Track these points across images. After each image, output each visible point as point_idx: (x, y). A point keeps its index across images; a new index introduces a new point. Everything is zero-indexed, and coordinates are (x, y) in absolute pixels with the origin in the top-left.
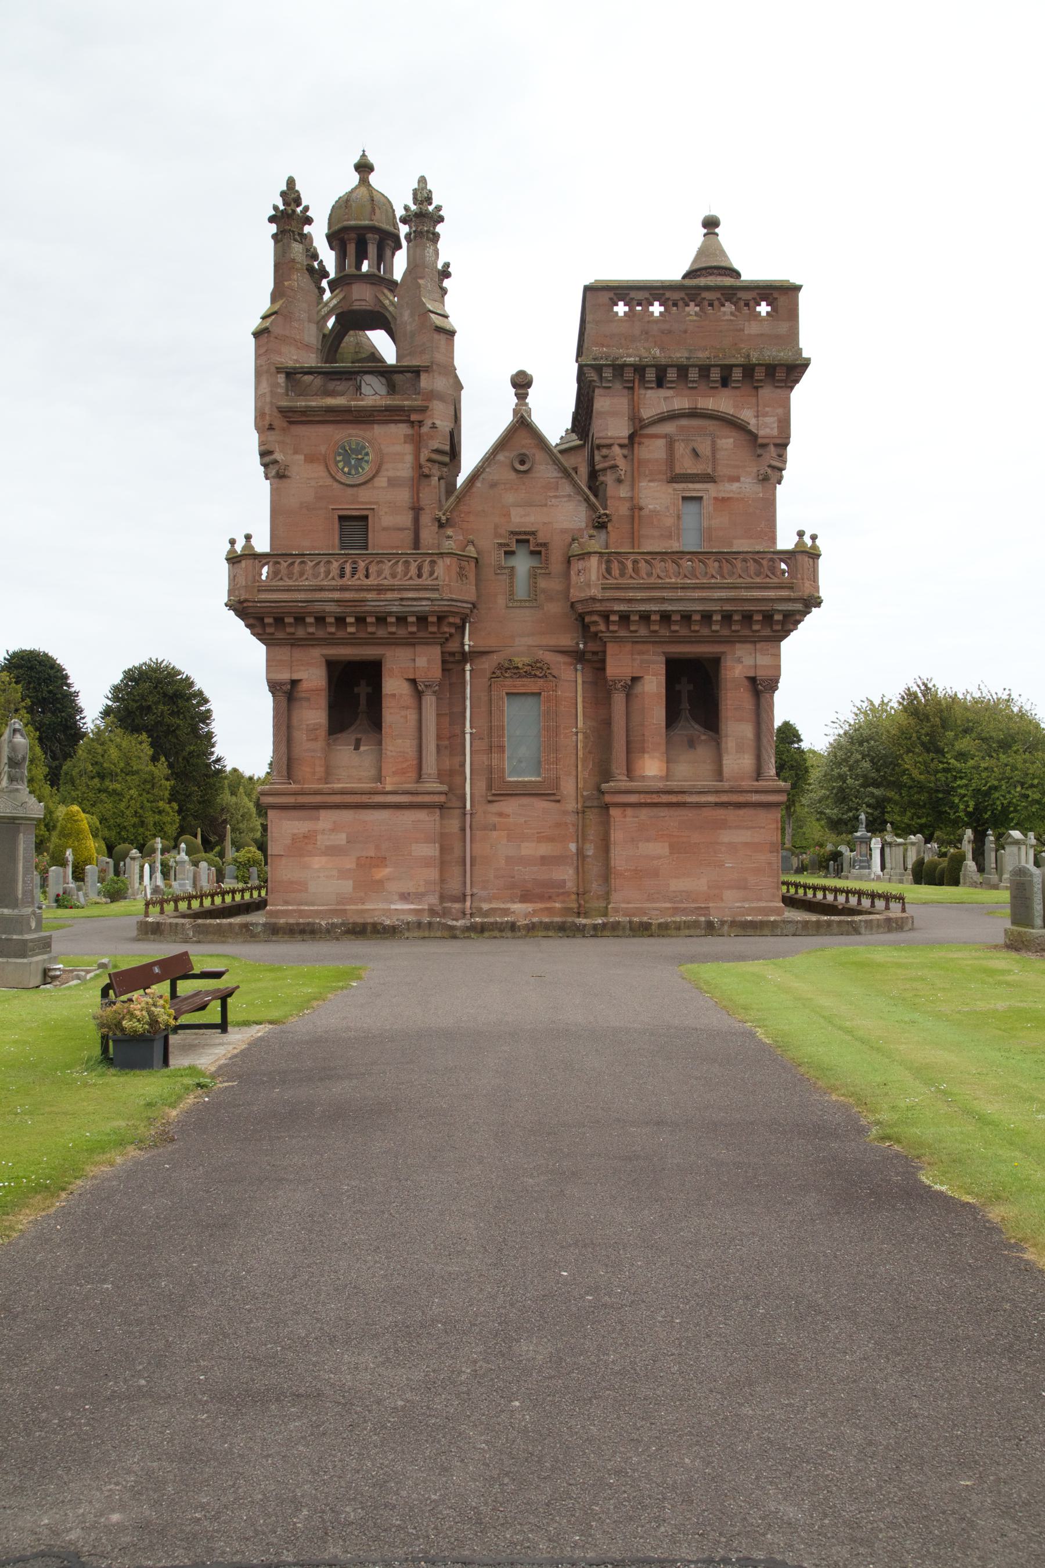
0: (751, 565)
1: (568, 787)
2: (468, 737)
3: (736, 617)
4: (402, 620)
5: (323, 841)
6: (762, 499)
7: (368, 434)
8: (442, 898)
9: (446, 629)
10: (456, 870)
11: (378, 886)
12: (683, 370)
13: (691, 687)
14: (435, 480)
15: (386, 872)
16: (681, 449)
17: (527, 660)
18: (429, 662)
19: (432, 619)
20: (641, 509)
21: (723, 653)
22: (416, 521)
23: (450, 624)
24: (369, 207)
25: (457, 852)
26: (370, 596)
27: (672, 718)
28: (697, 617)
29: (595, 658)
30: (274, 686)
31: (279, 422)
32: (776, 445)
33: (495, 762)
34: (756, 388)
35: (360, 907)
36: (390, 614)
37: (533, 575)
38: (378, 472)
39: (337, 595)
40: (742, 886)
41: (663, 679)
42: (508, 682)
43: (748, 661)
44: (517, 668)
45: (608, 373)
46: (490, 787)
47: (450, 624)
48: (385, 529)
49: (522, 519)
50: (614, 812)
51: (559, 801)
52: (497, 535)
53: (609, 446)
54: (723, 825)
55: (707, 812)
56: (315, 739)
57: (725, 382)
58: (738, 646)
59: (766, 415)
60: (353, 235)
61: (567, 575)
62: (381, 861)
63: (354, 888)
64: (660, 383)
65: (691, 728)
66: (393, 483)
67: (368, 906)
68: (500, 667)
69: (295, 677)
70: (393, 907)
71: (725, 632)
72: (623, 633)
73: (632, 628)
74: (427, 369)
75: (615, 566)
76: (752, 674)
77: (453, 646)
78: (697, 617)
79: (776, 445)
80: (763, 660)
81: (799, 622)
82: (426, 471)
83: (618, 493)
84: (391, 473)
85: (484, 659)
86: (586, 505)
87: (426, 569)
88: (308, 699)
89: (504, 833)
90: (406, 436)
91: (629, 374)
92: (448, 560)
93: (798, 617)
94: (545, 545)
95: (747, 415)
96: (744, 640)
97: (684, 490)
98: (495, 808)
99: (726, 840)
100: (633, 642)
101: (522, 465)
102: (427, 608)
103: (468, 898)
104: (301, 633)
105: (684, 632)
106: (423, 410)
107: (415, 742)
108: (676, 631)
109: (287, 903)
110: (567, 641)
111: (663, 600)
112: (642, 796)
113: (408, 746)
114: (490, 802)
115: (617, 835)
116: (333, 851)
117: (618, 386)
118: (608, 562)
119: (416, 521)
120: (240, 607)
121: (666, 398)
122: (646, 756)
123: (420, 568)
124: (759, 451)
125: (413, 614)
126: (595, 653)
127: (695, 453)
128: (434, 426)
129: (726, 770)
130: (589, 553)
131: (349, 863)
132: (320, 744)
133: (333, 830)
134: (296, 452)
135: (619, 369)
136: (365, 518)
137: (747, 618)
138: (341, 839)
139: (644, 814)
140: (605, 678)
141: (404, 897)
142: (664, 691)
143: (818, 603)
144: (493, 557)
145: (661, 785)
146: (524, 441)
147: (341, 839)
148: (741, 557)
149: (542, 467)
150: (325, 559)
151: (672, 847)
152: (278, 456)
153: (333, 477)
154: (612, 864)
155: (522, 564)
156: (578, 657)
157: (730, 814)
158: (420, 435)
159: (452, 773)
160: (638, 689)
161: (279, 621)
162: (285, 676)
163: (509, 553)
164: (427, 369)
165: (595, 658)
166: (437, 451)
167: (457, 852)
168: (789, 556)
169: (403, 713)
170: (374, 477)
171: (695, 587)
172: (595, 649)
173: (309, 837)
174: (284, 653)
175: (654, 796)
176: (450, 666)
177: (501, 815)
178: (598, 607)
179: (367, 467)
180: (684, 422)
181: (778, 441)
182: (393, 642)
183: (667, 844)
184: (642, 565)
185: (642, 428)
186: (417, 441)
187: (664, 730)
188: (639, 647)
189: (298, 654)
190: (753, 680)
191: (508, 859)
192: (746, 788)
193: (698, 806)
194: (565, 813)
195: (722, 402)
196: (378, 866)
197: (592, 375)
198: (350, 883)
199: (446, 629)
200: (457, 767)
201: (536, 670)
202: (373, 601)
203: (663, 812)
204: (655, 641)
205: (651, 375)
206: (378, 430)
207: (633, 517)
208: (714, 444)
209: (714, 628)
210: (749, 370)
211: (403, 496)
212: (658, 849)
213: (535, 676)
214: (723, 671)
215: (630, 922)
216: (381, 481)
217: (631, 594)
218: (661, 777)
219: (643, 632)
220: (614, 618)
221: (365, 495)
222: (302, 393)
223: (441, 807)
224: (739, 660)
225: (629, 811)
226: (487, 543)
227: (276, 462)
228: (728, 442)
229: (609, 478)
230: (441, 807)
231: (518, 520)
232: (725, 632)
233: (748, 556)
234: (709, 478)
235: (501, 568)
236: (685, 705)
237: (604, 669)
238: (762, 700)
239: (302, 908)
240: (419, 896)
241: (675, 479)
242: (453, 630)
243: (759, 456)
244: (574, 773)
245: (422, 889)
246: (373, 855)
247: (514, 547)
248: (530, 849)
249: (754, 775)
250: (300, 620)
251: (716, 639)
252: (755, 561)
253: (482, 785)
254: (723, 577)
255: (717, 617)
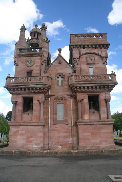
0: (104, 77)
1: (69, 121)
2: (49, 112)
3: (102, 87)
4: (36, 89)
5: (20, 132)
6: (104, 67)
7: (33, 58)
8: (44, 144)
9: (45, 91)
10: (47, 139)
11: (31, 142)
12: (88, 46)
13: (92, 103)
14: (44, 65)
15: (32, 139)
16: (88, 59)
17: (61, 97)
18: (42, 97)
19: (42, 89)
20: (82, 69)
21: (99, 94)
22: (40, 72)
23: (46, 90)
24: (36, 29)
25: (47, 135)
26: (30, 84)
27: (90, 108)
28: (94, 87)
29: (74, 96)
30: (13, 102)
31: (17, 57)
32: (106, 58)
33: (55, 117)
34: (101, 49)
35: (27, 146)
36: (34, 88)
37: (62, 81)
38: (34, 64)
39: (24, 84)
40: (106, 141)
41: (88, 100)
42: (57, 101)
43: (104, 96)
44: (59, 98)
45: (75, 46)
46: (54, 122)
47: (46, 90)
48: (35, 74)
49: (60, 71)
50: (79, 126)
51: (68, 124)
52: (55, 74)
53: (75, 58)
54: (101, 128)
55: (98, 126)
56: (20, 112)
57: (95, 48)
58: (102, 93)
59: (103, 53)
60: (33, 33)
61: (68, 81)
62: (31, 137)
63: (26, 142)
64: (84, 48)
65: (92, 110)
66: (36, 66)
67: (29, 146)
68: (56, 98)
69: (17, 100)
70: (34, 146)
71: (99, 90)
72: (79, 91)
73: (82, 90)
74: (43, 47)
75: (78, 78)
76: (105, 98)
77: (47, 94)
78: (94, 87)
79: (106, 58)
80: (107, 95)
81: (113, 88)
82: (42, 64)
83: (77, 67)
84: (36, 64)
85: (53, 97)
86: (71, 69)
87: (41, 79)
88: (19, 104)
89: (56, 131)
90: (39, 58)
91: (78, 46)
92: (45, 77)
93: (113, 87)
94: (64, 76)
95: (100, 53)
96: (103, 92)
97: (89, 66)
98: (54, 126)
99: (102, 131)
100: (82, 93)
101: (60, 62)
102: (41, 86)
103: (49, 145)
104: (18, 92)
105: (91, 90)
106: (42, 54)
107: (39, 113)
108: (90, 90)
109: (12, 145)
110: (69, 93)
111: (87, 84)
112: (85, 123)
113: (38, 114)
114: (54, 125)
115: (80, 131)
116: (22, 135)
117: (76, 49)
118: (76, 77)
119: (40, 72)
120: (8, 87)
121: (85, 51)
122: (85, 115)
123: (40, 79)
124: (103, 59)
125: (39, 87)
126: (74, 95)
127: (91, 59)
128: (44, 56)
129: (101, 117)
130: (72, 75)
131: (25, 137)
132: (20, 113)
133: (22, 130)
134: (20, 62)
135: (76, 46)
136: (31, 72)
137: (104, 87)
138: (23, 132)
139: (85, 126)
140: (77, 100)
141: (36, 144)
142: (88, 102)
143: (117, 84)
144: (54, 78)
145: (88, 121)
146: (60, 59)
147: (23, 132)
148: (102, 75)
149: (64, 63)
150: (22, 78)
151: (91, 133)
152: (16, 62)
153: (26, 65)
154: (79, 137)
155: (60, 79)
156: (71, 96)
157: (103, 126)
158: (42, 58)
159: (46, 119)
160: (83, 102)
161: (14, 89)
162: (15, 100)
163: (58, 78)
164: (43, 47)
165: (74, 96)
166: (44, 60)
167: (47, 135)
168: (110, 75)
169: (37, 107)
170: (33, 65)
171: (93, 81)
172: (74, 94)
173: (17, 132)
174: (15, 96)
175: (87, 123)
176: (46, 99)
177: (56, 127)
178: (74, 85)
179: (32, 64)
180: (89, 55)
181: (106, 57)
182: (35, 93)
183: (90, 133)
184: (83, 77)
185: (81, 56)
186: (41, 59)
187: (88, 110)
188: (82, 94)
189: (18, 96)
190: (105, 99)
191: (58, 137)
192: (106, 121)
193: (96, 125)
194: (69, 127)
195: (95, 51)
196: (30, 138)
197: (72, 47)
198: (25, 141)
199: (45, 91)
200: (48, 118)
201: (63, 99)
202: (31, 86)
203: (89, 126)
204: (86, 92)
205: (82, 46)
206: (34, 58)
207: (80, 70)
208: (94, 58)
209: (97, 89)
210: (99, 45)
211: (38, 68)
212: (88, 134)
213: (63, 100)
214: (99, 98)
215: (84, 151)
216: (34, 66)
217: (81, 83)
218: (88, 119)
219: (83, 90)
220: (78, 88)
221: (31, 68)
222: (22, 52)
223: (44, 126)
224: (102, 96)
225: (82, 126)
226: (54, 76)
227: (16, 63)
228: (97, 58)
229: (76, 64)
230: (44, 126)
231: (59, 72)
232: (99, 90)
233: (103, 75)
234: (94, 64)
235: (56, 80)
236: (92, 106)
237: (76, 98)
238: (107, 103)
239: (16, 146)
240: (39, 144)
241: (88, 64)
242: (46, 91)
243: (103, 60)
244: (71, 119)
245: (39, 143)
246: (30, 135)
247: (58, 76)
248: (62, 134)
249: (107, 118)
250: (17, 89)
251: (98, 92)
252: (104, 76)
253: (52, 121)
254: (98, 79)
255: (98, 87)
